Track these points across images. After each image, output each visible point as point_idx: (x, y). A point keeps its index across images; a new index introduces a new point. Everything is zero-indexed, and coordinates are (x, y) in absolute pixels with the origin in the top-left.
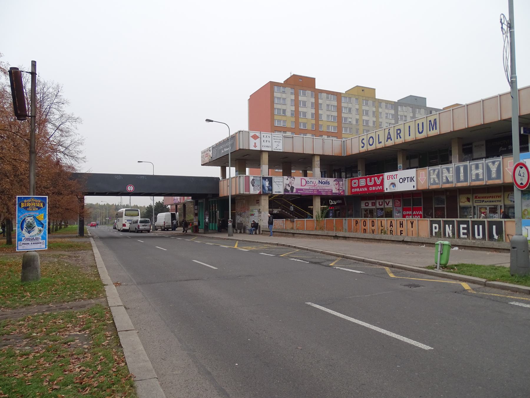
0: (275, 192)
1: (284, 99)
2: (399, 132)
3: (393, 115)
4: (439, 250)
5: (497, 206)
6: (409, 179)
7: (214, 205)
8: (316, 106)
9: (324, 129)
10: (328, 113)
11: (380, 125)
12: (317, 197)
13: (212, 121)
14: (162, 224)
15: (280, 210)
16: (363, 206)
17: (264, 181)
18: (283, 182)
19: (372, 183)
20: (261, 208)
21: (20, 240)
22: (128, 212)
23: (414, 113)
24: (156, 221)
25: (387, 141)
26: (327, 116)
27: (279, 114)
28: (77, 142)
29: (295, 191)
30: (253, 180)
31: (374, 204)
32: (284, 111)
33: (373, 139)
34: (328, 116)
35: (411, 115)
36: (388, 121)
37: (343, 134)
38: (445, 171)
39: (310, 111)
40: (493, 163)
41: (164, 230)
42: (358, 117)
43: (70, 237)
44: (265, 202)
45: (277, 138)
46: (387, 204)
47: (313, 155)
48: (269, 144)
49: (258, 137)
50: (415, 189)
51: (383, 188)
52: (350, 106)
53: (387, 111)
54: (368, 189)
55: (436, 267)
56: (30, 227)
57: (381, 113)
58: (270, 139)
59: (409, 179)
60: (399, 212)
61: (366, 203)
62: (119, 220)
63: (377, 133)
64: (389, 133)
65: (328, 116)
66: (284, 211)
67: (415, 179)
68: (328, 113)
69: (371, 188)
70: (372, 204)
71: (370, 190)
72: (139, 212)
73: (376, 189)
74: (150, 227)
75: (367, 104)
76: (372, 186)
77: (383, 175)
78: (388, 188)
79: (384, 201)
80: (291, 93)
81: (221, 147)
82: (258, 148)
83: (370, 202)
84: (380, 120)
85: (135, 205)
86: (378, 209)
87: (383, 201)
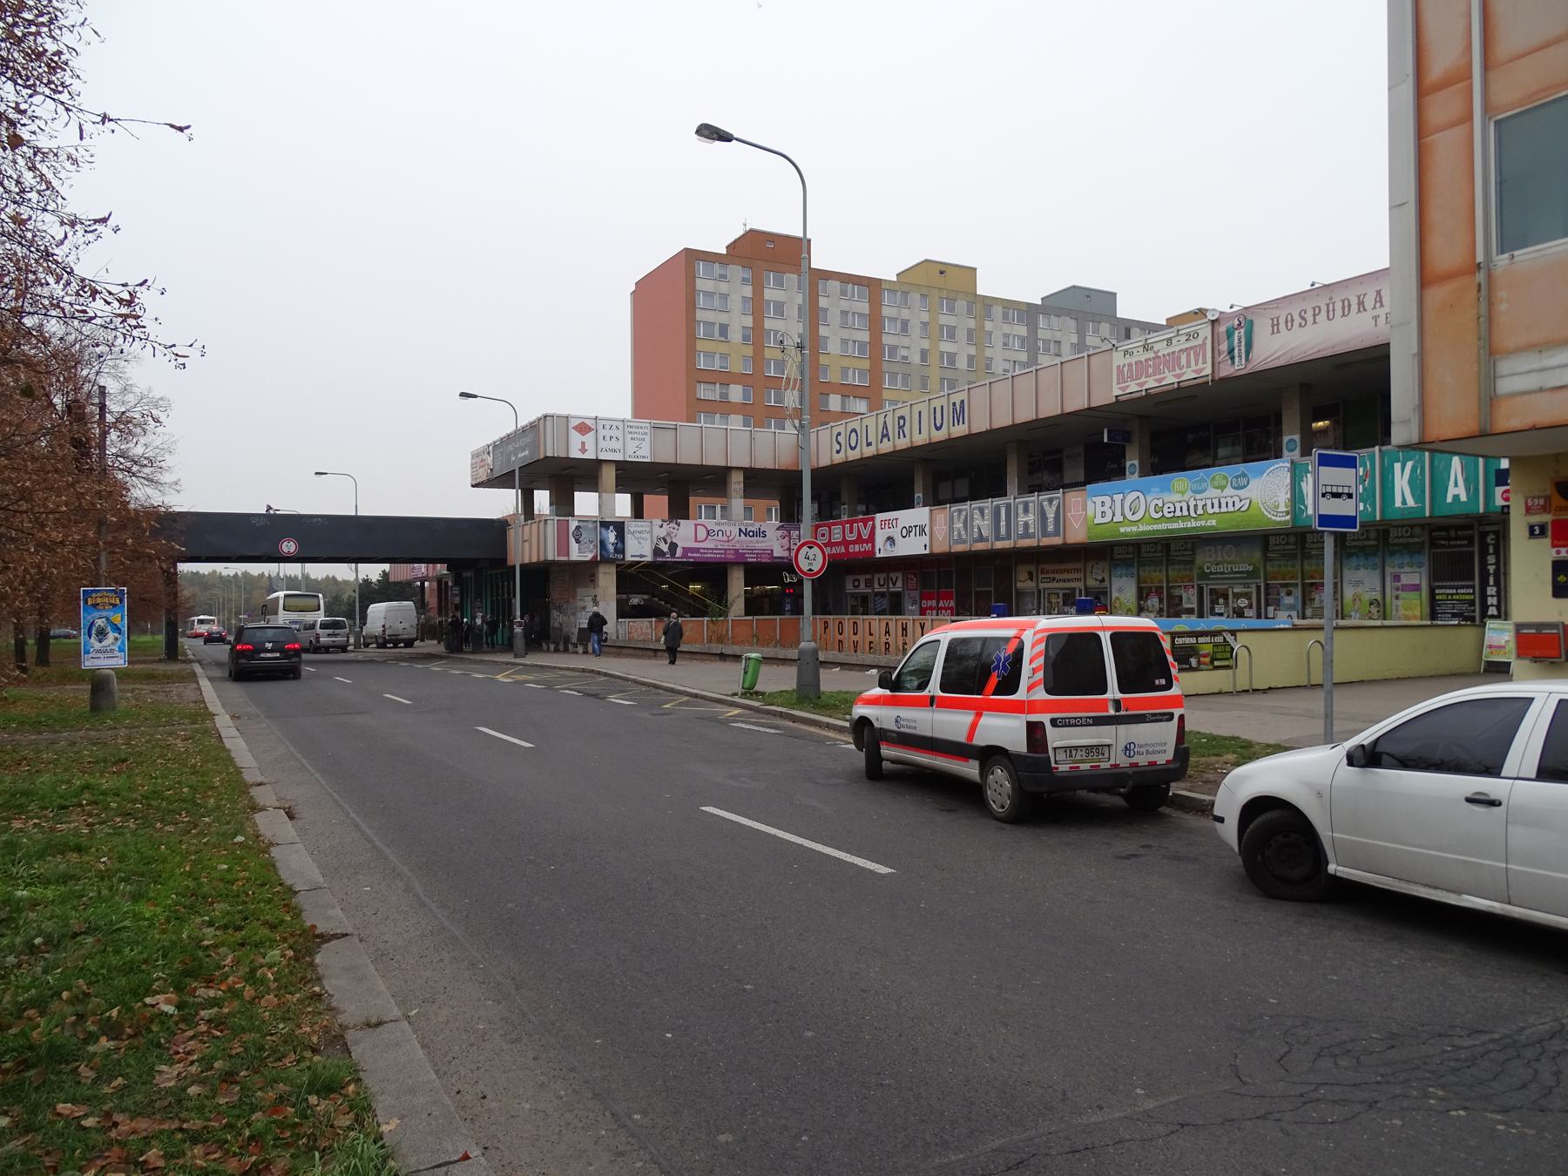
0: (632, 556)
1: (724, 297)
2: (902, 422)
3: (1022, 340)
4: (743, 666)
5: (1074, 589)
6: (918, 528)
7: (506, 583)
8: (813, 315)
9: (833, 376)
10: (845, 334)
11: (988, 366)
12: (735, 567)
13: (476, 396)
14: (378, 630)
15: (646, 597)
16: (849, 588)
17: (603, 530)
18: (651, 532)
20: (599, 592)
21: (87, 652)
22: (292, 601)
23: (1081, 333)
24: (364, 625)
25: (881, 442)
26: (842, 342)
27: (709, 337)
28: (160, 447)
29: (679, 552)
30: (578, 528)
31: (869, 584)
32: (724, 329)
33: (857, 436)
34: (844, 342)
35: (1074, 339)
36: (1008, 354)
37: (884, 392)
38: (977, 514)
39: (792, 328)
40: (1050, 501)
41: (382, 646)
42: (926, 344)
43: (145, 662)
44: (607, 580)
45: (637, 430)
46: (894, 584)
47: (728, 469)
48: (618, 445)
49: (590, 429)
50: (927, 552)
51: (873, 546)
52: (905, 314)
53: (1006, 329)
54: (847, 549)
55: (737, 695)
56: (102, 634)
57: (990, 334)
58: (618, 434)
59: (918, 528)
60: (914, 603)
61: (854, 581)
62: (269, 619)
63: (916, 409)
64: (885, 423)
65: (844, 342)
66: (656, 599)
67: (927, 530)
68: (845, 334)
70: (866, 583)
72: (322, 602)
74: (348, 637)
75: (951, 309)
76: (854, 542)
77: (873, 519)
78: (883, 550)
79: (888, 576)
80: (744, 279)
81: (511, 448)
82: (590, 455)
83: (862, 578)
84: (988, 352)
85: (328, 576)
86: (877, 594)
87: (885, 575)
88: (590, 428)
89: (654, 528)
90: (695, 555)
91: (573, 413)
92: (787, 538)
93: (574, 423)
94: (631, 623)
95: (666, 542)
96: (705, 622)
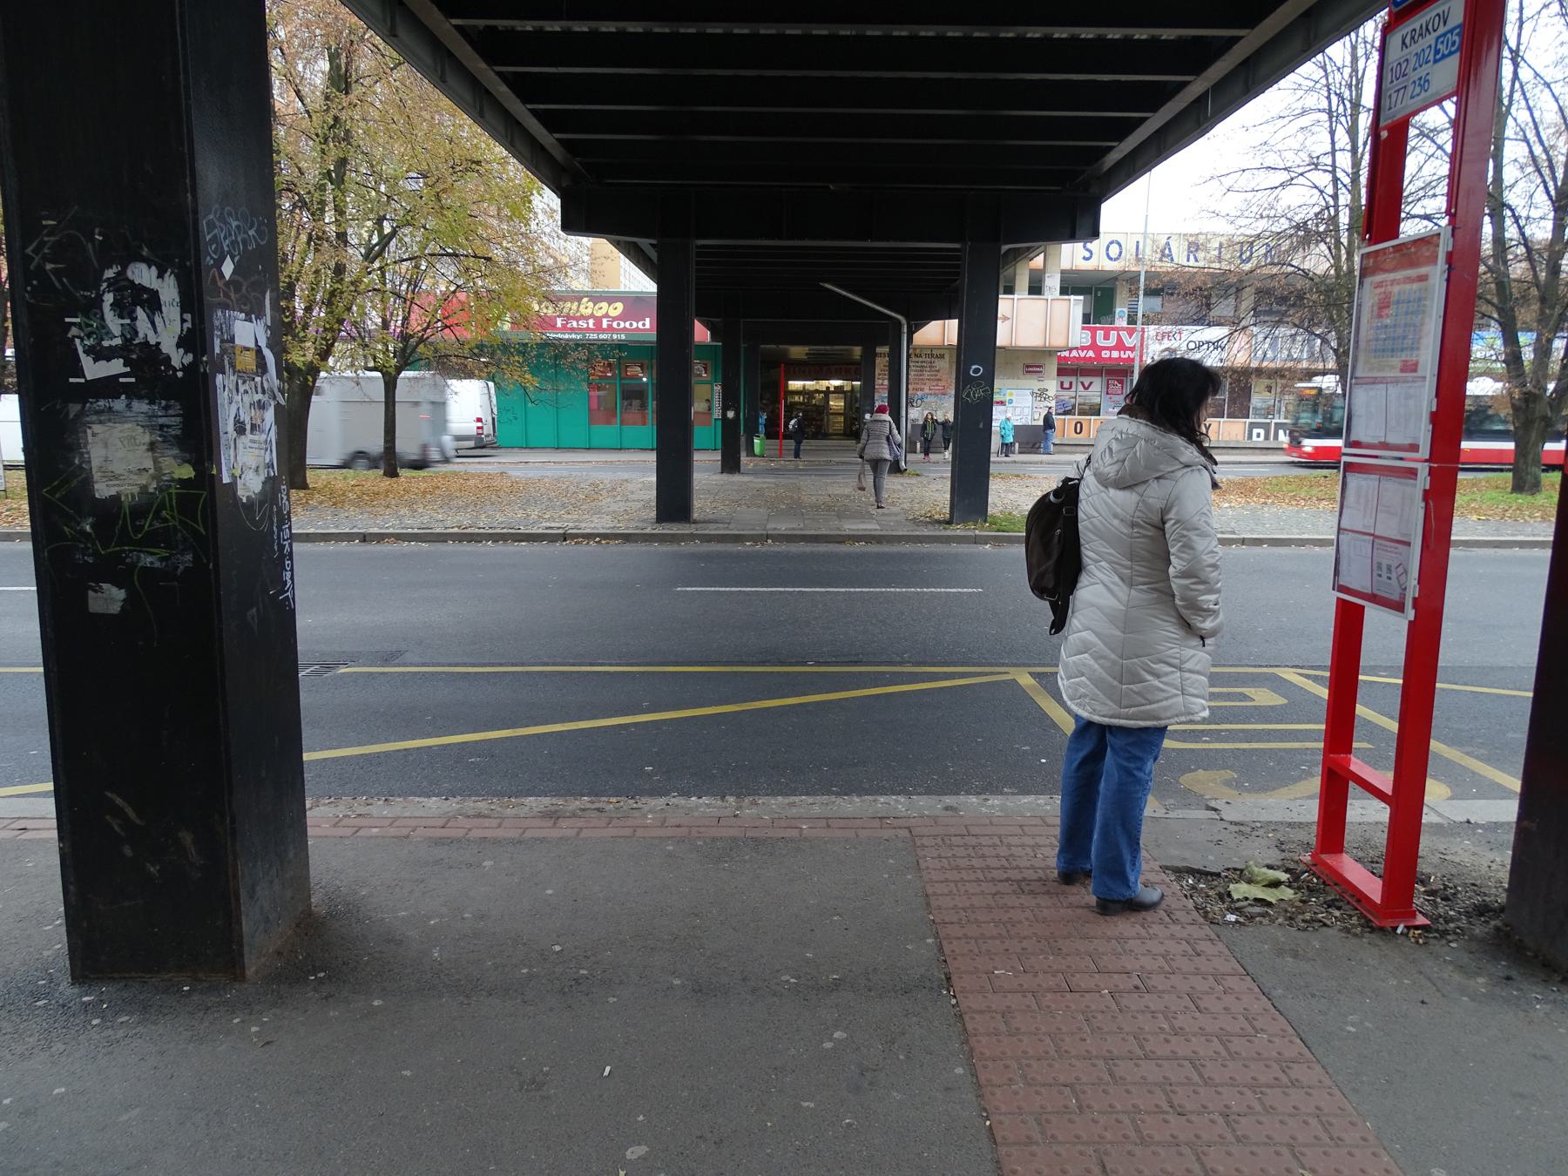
19: (1112, 342)
69: (1108, 352)
71: (1103, 356)
73: (1123, 356)
76: (1110, 349)
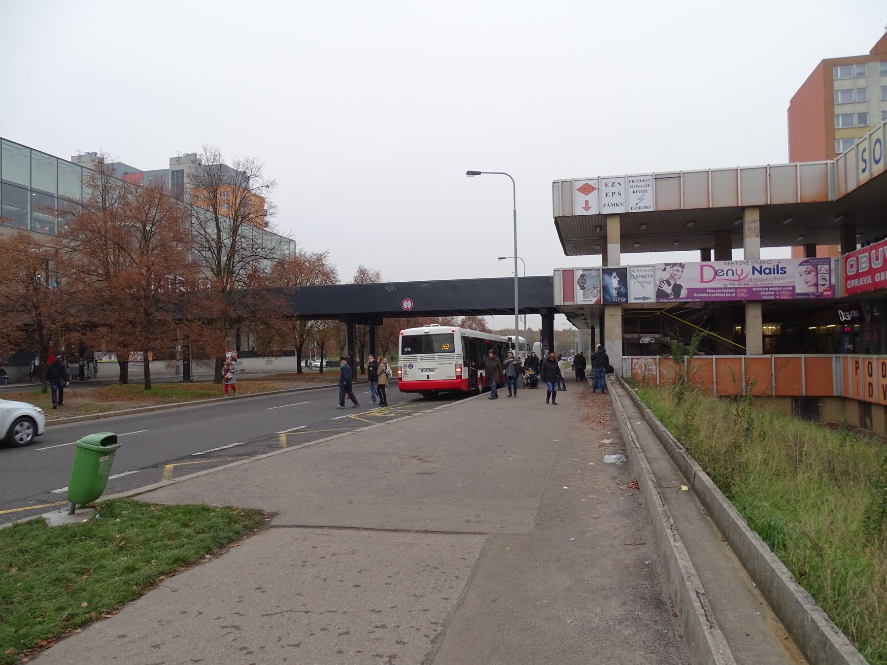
0: (635, 299)
13: (479, 173)
15: (657, 336)
17: (606, 277)
29: (683, 293)
30: (582, 276)
32: (863, 117)
45: (639, 184)
48: (616, 199)
49: (593, 189)
54: (873, 279)
82: (593, 211)
88: (593, 187)
89: (657, 271)
90: (702, 295)
91: (576, 177)
92: (813, 273)
93: (579, 185)
94: (635, 360)
95: (669, 284)
96: (657, 360)
